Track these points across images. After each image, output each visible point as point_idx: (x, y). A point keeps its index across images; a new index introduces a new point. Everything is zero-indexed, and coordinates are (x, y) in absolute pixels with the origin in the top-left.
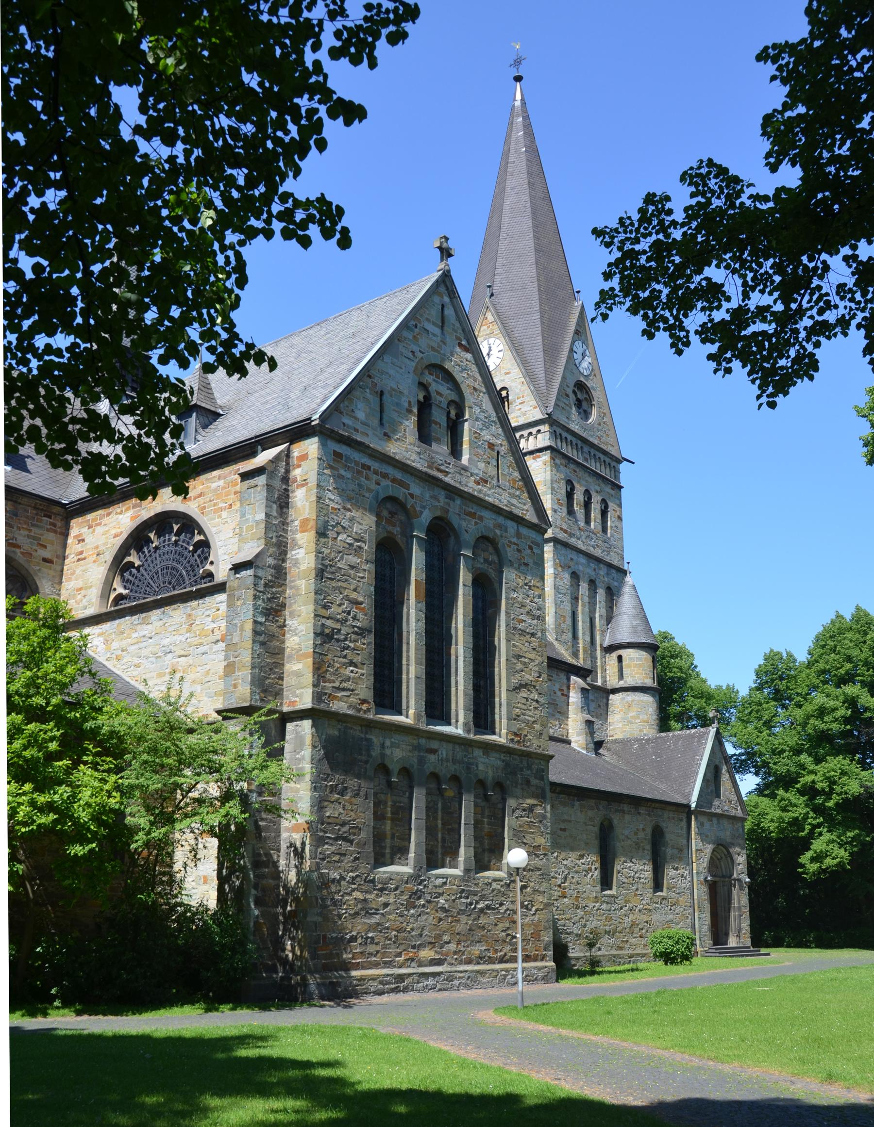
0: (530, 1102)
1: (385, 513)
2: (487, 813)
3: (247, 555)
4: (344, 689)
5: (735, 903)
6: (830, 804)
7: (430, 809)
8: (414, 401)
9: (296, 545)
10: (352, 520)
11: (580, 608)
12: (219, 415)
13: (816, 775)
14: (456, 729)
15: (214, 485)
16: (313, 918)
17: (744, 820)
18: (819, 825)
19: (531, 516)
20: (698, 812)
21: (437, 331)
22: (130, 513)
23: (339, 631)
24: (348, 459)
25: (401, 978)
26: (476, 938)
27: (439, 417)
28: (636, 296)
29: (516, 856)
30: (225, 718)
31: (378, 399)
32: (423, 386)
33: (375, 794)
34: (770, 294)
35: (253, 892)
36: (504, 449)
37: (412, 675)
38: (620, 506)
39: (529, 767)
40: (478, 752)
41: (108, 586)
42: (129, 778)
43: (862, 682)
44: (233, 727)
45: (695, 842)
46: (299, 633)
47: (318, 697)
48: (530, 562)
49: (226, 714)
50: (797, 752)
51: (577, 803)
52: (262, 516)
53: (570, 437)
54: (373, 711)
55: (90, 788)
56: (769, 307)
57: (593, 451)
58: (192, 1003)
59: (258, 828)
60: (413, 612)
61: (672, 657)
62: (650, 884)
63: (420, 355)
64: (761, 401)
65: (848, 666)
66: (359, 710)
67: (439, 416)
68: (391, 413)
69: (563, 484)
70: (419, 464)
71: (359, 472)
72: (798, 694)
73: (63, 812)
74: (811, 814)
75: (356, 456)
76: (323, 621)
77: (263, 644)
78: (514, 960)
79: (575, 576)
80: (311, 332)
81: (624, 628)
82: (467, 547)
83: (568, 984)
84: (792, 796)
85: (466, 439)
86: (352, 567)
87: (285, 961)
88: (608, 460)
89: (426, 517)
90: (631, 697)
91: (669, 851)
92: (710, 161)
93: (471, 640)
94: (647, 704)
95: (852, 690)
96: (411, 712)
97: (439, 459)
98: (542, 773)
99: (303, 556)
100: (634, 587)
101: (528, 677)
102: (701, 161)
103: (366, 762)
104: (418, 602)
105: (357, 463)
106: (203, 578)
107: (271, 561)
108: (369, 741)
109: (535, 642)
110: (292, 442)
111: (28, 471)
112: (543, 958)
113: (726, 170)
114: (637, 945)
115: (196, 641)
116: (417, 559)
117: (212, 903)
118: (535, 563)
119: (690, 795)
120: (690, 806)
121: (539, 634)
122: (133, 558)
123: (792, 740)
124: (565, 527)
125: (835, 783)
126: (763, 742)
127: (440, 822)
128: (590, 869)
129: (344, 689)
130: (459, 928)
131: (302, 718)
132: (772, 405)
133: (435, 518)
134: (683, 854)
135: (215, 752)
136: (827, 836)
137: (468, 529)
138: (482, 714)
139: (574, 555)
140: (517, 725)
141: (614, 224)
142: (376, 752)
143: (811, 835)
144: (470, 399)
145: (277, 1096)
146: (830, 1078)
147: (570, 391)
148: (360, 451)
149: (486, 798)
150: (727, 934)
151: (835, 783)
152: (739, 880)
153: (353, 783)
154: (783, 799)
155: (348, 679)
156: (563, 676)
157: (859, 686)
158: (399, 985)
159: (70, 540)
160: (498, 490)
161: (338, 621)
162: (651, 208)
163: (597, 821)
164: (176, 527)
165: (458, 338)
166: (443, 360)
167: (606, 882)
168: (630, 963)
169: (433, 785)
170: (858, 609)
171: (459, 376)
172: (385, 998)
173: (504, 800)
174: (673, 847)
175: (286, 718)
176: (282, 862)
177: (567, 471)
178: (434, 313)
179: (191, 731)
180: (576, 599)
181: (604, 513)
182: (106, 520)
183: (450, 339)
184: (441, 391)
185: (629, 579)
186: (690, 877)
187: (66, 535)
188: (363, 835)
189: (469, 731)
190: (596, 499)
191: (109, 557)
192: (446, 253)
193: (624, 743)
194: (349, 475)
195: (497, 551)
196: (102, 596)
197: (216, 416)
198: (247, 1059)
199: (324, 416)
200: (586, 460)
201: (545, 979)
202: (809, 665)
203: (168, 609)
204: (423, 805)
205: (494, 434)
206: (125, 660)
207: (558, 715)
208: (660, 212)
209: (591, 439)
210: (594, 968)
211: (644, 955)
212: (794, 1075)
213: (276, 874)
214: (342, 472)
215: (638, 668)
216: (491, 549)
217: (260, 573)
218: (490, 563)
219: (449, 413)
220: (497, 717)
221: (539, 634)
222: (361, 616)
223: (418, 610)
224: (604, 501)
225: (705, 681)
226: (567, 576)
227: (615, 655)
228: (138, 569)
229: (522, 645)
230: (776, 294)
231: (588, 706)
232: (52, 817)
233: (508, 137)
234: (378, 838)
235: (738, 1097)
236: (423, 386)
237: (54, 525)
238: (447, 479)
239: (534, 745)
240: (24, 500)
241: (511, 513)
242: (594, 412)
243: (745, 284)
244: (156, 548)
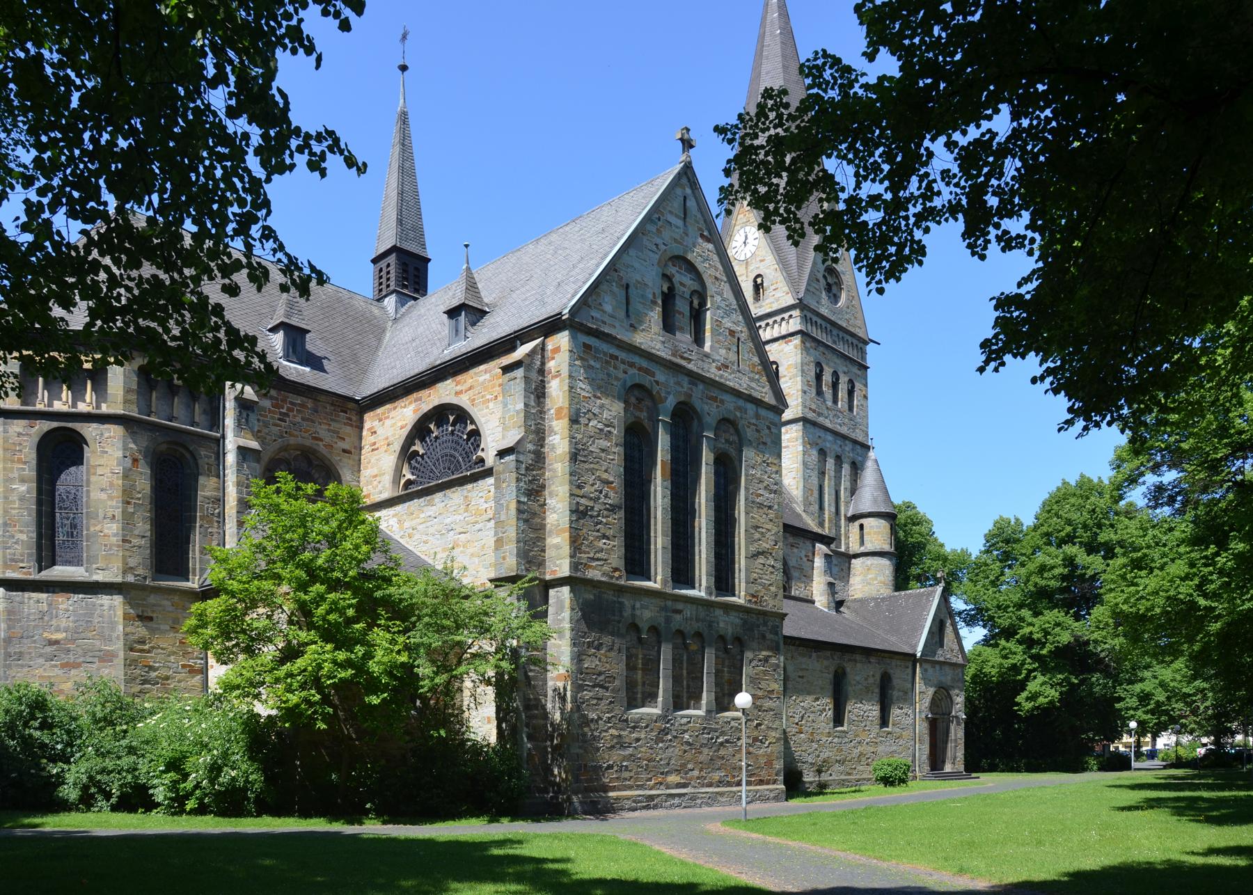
0: (703, 888)
1: (633, 400)
2: (727, 663)
3: (509, 442)
4: (598, 559)
5: (952, 736)
6: (1044, 652)
7: (676, 661)
8: (658, 292)
9: (552, 432)
10: (602, 407)
11: (826, 482)
12: (484, 313)
13: (1033, 626)
14: (699, 593)
15: (481, 379)
16: (575, 750)
17: (963, 666)
18: (1035, 670)
19: (769, 398)
20: (922, 660)
21: (680, 223)
22: (412, 407)
23: (592, 508)
25: (651, 798)
26: (712, 766)
27: (684, 306)
28: (756, 191)
29: (743, 699)
30: (496, 586)
32: (667, 277)
33: (628, 649)
34: (881, 182)
35: (525, 729)
36: (744, 336)
37: (659, 546)
38: (866, 385)
39: (765, 624)
40: (719, 612)
41: (398, 473)
42: (415, 638)
43: (1081, 543)
44: (502, 593)
45: (919, 685)
46: (557, 511)
47: (575, 566)
48: (769, 441)
49: (498, 582)
50: (1020, 606)
51: (814, 655)
52: (521, 406)
53: (819, 321)
54: (624, 578)
55: (384, 648)
56: (880, 195)
57: (841, 334)
58: (478, 817)
59: (527, 677)
60: (659, 489)
61: (914, 524)
62: (877, 721)
63: (663, 247)
64: (871, 287)
65: (1069, 529)
66: (612, 577)
67: (682, 306)
68: (636, 305)
69: (812, 367)
70: (664, 353)
71: (607, 362)
72: (1022, 555)
73: (359, 667)
74: (1029, 660)
75: (604, 347)
76: (578, 499)
77: (526, 521)
78: (739, 784)
79: (822, 453)
80: (567, 229)
81: (866, 500)
82: (709, 430)
83: (796, 802)
84: (1012, 645)
85: (708, 327)
86: (603, 450)
87: (554, 784)
88: (855, 342)
89: (671, 402)
90: (870, 561)
91: (895, 694)
92: (824, 51)
93: (712, 513)
94: (885, 568)
95: (1070, 549)
96: (659, 578)
97: (682, 347)
98: (777, 629)
99: (558, 442)
100: (876, 461)
101: (765, 545)
102: (816, 53)
104: (664, 480)
105: (605, 354)
106: (476, 463)
107: (530, 447)
108: (621, 603)
109: (772, 514)
110: (546, 336)
111: (324, 371)
112: (775, 782)
113: (838, 61)
114: (865, 771)
115: (472, 519)
116: (663, 441)
117: (493, 739)
118: (773, 442)
119: (916, 645)
120: (915, 655)
121: (776, 507)
122: (418, 447)
123: (1016, 598)
124: (813, 407)
125: (1049, 634)
126: (989, 598)
127: (685, 672)
129: (598, 559)
130: (701, 758)
131: (562, 585)
132: (881, 291)
133: (679, 403)
134: (907, 696)
135: (486, 614)
136: (1041, 679)
137: (710, 411)
138: (723, 579)
139: (822, 433)
140: (755, 588)
141: (734, 121)
142: (627, 613)
143: (1027, 678)
144: (711, 288)
145: (510, 882)
146: (962, 871)
148: (608, 342)
149: (726, 651)
150: (944, 762)
151: (1049, 634)
152: (957, 717)
153: (607, 640)
154: (1004, 648)
155: (602, 550)
156: (808, 544)
157: (1077, 546)
158: (650, 803)
159: (364, 433)
160: (738, 375)
161: (591, 499)
162: (770, 103)
163: (832, 669)
164: (451, 418)
165: (700, 229)
166: (686, 252)
167: (838, 719)
168: (856, 786)
169: (679, 641)
170: (1082, 476)
171: (701, 267)
172: (637, 813)
173: (742, 653)
175: (548, 585)
176: (549, 706)
177: (816, 354)
178: (676, 205)
179: (467, 597)
180: (823, 473)
181: (851, 393)
182: (393, 414)
183: (692, 230)
184: (684, 282)
185: (872, 454)
186: (911, 718)
187: (361, 428)
188: (617, 683)
189: (711, 594)
190: (843, 380)
191: (397, 447)
192: (687, 144)
193: (862, 602)
195: (737, 431)
196: (394, 482)
197: (483, 313)
198: (499, 857)
199: (574, 310)
200: (834, 342)
201: (776, 799)
202: (1036, 528)
203: (448, 492)
204: (670, 657)
205: (733, 321)
206: (416, 537)
207: (804, 579)
208: (775, 107)
209: (840, 322)
210: (822, 789)
211: (869, 779)
212: (935, 869)
213: (545, 715)
214: (592, 363)
215: (877, 535)
216: (732, 430)
217: (522, 458)
219: (692, 303)
220: (737, 581)
221: (776, 507)
222: (612, 494)
223: (664, 487)
224: (851, 382)
225: (942, 546)
226: (815, 453)
227: (857, 524)
228: (422, 456)
229: (760, 517)
230: (886, 183)
231: (830, 568)
232: (350, 672)
233: (764, 18)
234: (630, 685)
235: (876, 885)
236: (667, 277)
237: (350, 419)
238: (690, 366)
239: (770, 604)
240: (322, 398)
241: (750, 396)
242: (844, 295)
243: (857, 175)
244: (436, 438)
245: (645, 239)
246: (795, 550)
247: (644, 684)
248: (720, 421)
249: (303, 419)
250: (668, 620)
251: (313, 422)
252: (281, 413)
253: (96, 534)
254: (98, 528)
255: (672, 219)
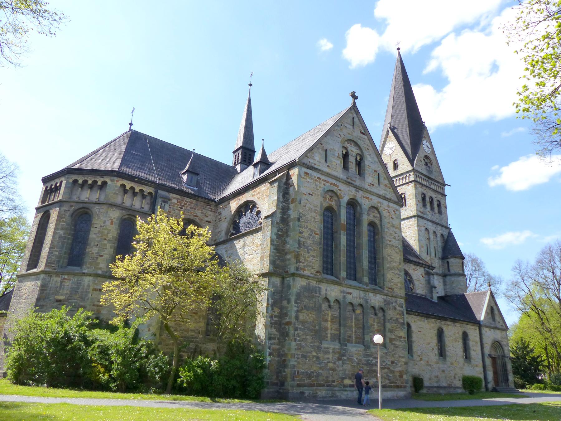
1: (328, 197)
2: (376, 320)
21: (351, 127)
24: (311, 175)
31: (325, 153)
35: (268, 350)
51: (426, 320)
52: (276, 198)
53: (423, 177)
57: (433, 182)
88: (439, 185)
103: (319, 297)
105: (315, 177)
115: (255, 248)
127: (354, 324)
128: (433, 349)
142: (323, 292)
144: (365, 153)
147: (422, 159)
163: (436, 329)
174: (473, 341)
177: (421, 190)
178: (350, 120)
184: (353, 150)
194: (311, 181)
216: (376, 212)
218: (376, 217)
219: (356, 158)
236: (345, 148)
245: (335, 132)
246: (416, 272)
247: (331, 329)
248: (370, 208)
249: (190, 208)
250: (344, 297)
251: (195, 209)
252: (181, 205)
253: (88, 252)
254: (89, 250)
255: (348, 126)
